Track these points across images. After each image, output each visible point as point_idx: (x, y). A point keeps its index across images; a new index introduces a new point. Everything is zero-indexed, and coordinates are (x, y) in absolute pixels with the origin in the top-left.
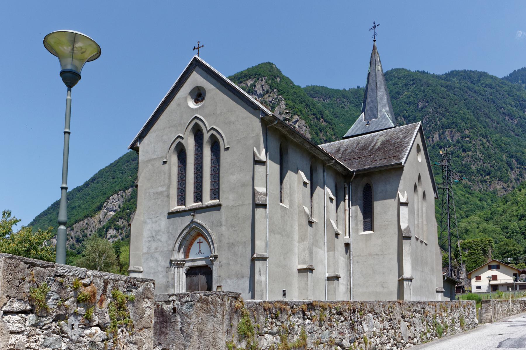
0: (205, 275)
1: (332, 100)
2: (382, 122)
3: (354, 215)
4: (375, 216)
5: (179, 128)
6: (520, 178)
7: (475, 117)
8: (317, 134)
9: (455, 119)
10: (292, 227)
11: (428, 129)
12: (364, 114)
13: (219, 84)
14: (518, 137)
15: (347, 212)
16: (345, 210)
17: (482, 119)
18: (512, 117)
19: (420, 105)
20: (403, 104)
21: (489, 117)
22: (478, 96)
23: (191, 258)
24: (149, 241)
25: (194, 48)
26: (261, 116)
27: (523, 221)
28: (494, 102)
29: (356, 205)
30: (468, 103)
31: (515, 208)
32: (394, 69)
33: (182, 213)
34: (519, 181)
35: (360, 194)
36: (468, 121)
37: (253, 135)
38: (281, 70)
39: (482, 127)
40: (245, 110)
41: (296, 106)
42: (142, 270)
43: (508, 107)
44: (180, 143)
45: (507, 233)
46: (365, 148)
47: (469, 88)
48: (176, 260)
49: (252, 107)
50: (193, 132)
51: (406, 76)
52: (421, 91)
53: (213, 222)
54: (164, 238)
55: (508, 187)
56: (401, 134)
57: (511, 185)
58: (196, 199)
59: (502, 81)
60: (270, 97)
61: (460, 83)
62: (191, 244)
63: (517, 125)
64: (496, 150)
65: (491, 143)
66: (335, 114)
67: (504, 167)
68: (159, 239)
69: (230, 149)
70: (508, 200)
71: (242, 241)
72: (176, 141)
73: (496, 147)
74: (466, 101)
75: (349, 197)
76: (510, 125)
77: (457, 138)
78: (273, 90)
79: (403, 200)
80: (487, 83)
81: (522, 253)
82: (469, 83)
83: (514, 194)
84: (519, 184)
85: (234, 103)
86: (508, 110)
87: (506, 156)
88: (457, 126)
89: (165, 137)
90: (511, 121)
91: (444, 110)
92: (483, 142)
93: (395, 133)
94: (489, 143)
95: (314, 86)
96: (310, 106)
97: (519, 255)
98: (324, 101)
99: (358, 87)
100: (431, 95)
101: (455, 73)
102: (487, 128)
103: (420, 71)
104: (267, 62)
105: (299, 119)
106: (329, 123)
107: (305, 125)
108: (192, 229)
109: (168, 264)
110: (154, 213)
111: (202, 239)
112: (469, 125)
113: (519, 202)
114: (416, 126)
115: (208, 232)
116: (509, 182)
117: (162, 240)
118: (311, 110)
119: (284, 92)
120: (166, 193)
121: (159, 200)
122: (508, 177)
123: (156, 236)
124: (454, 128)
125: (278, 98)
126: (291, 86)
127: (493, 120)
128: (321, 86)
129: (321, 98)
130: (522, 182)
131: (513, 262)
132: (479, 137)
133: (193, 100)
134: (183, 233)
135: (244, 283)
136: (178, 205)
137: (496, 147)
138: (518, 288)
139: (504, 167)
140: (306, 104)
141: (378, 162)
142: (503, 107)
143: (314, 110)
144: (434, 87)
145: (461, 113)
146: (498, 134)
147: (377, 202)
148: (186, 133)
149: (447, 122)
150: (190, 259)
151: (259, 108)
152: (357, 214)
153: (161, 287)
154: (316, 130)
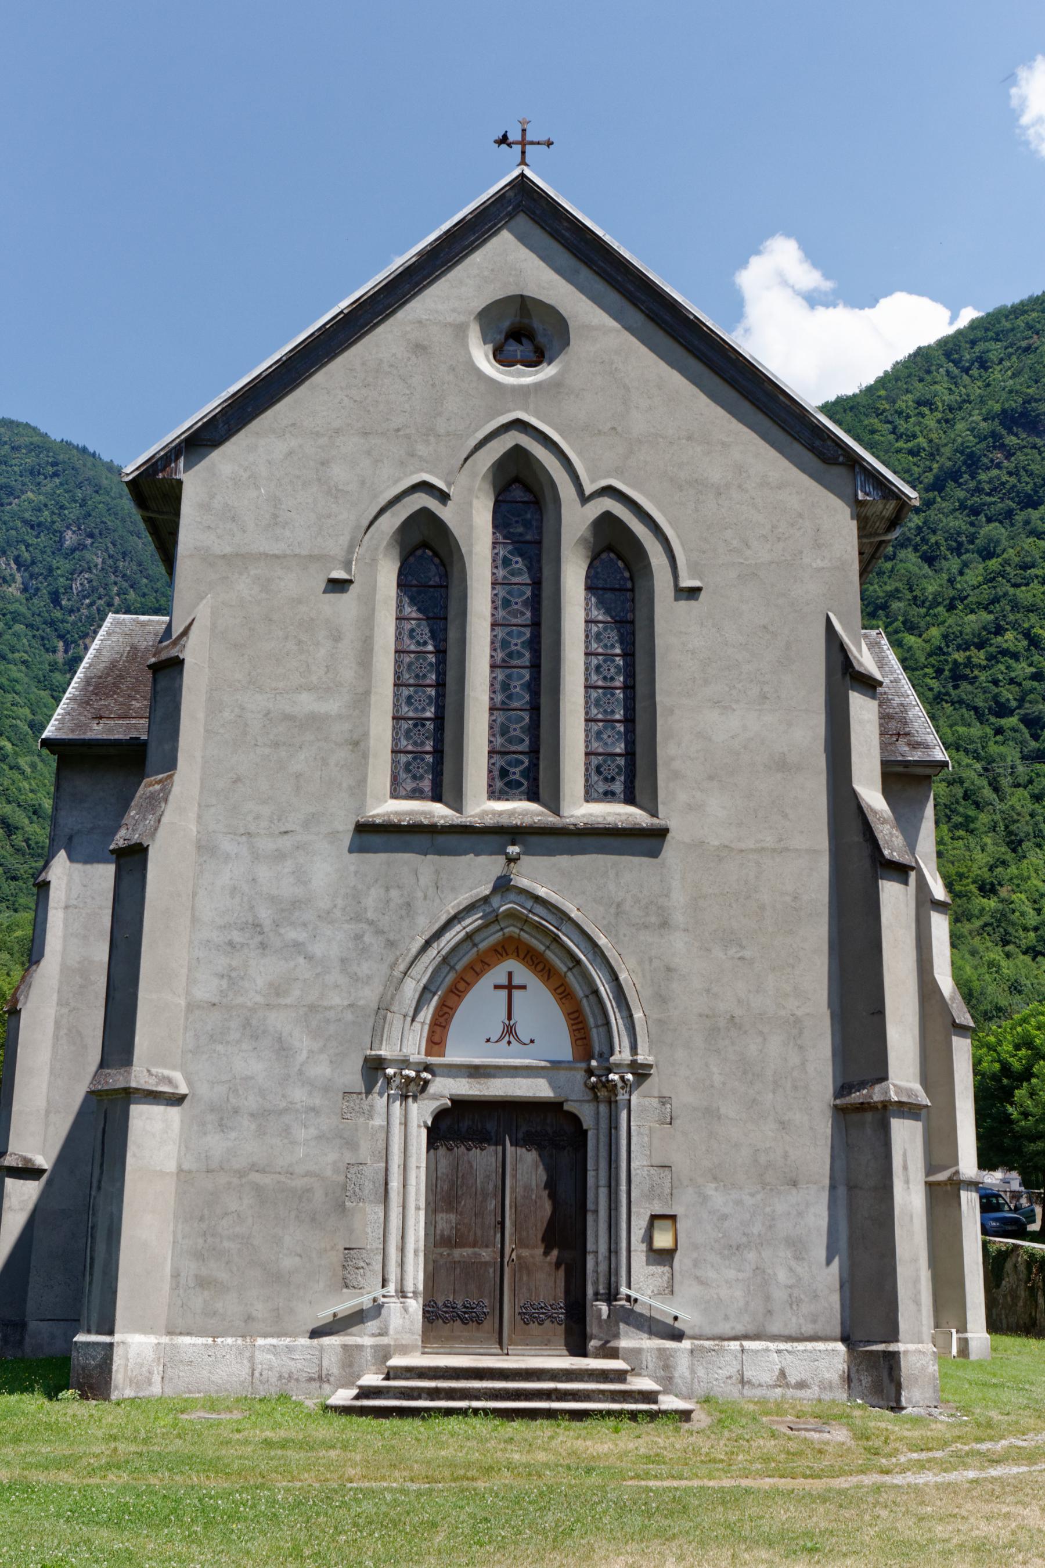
0: (540, 1148)
5: (422, 449)
11: (85, 611)
19: (70, 538)
20: (19, 524)
23: (453, 1056)
24: (231, 944)
25: (504, 140)
33: (441, 839)
37: (819, 563)
40: (773, 453)
42: (183, 1089)
48: (405, 1063)
49: (812, 449)
52: (75, 501)
53: (619, 905)
58: (499, 784)
62: (457, 991)
68: (297, 946)
69: (703, 594)
71: (783, 1013)
72: (407, 500)
89: (339, 473)
91: (135, 568)
100: (104, 519)
103: (75, 444)
109: (353, 1076)
111: (522, 974)
115: (595, 945)
134: (448, 936)
135: (800, 1214)
136: (395, 795)
144: (114, 499)
148: (463, 479)
149: (142, 603)
150: (447, 1059)
151: (854, 462)
153: (309, 1190)
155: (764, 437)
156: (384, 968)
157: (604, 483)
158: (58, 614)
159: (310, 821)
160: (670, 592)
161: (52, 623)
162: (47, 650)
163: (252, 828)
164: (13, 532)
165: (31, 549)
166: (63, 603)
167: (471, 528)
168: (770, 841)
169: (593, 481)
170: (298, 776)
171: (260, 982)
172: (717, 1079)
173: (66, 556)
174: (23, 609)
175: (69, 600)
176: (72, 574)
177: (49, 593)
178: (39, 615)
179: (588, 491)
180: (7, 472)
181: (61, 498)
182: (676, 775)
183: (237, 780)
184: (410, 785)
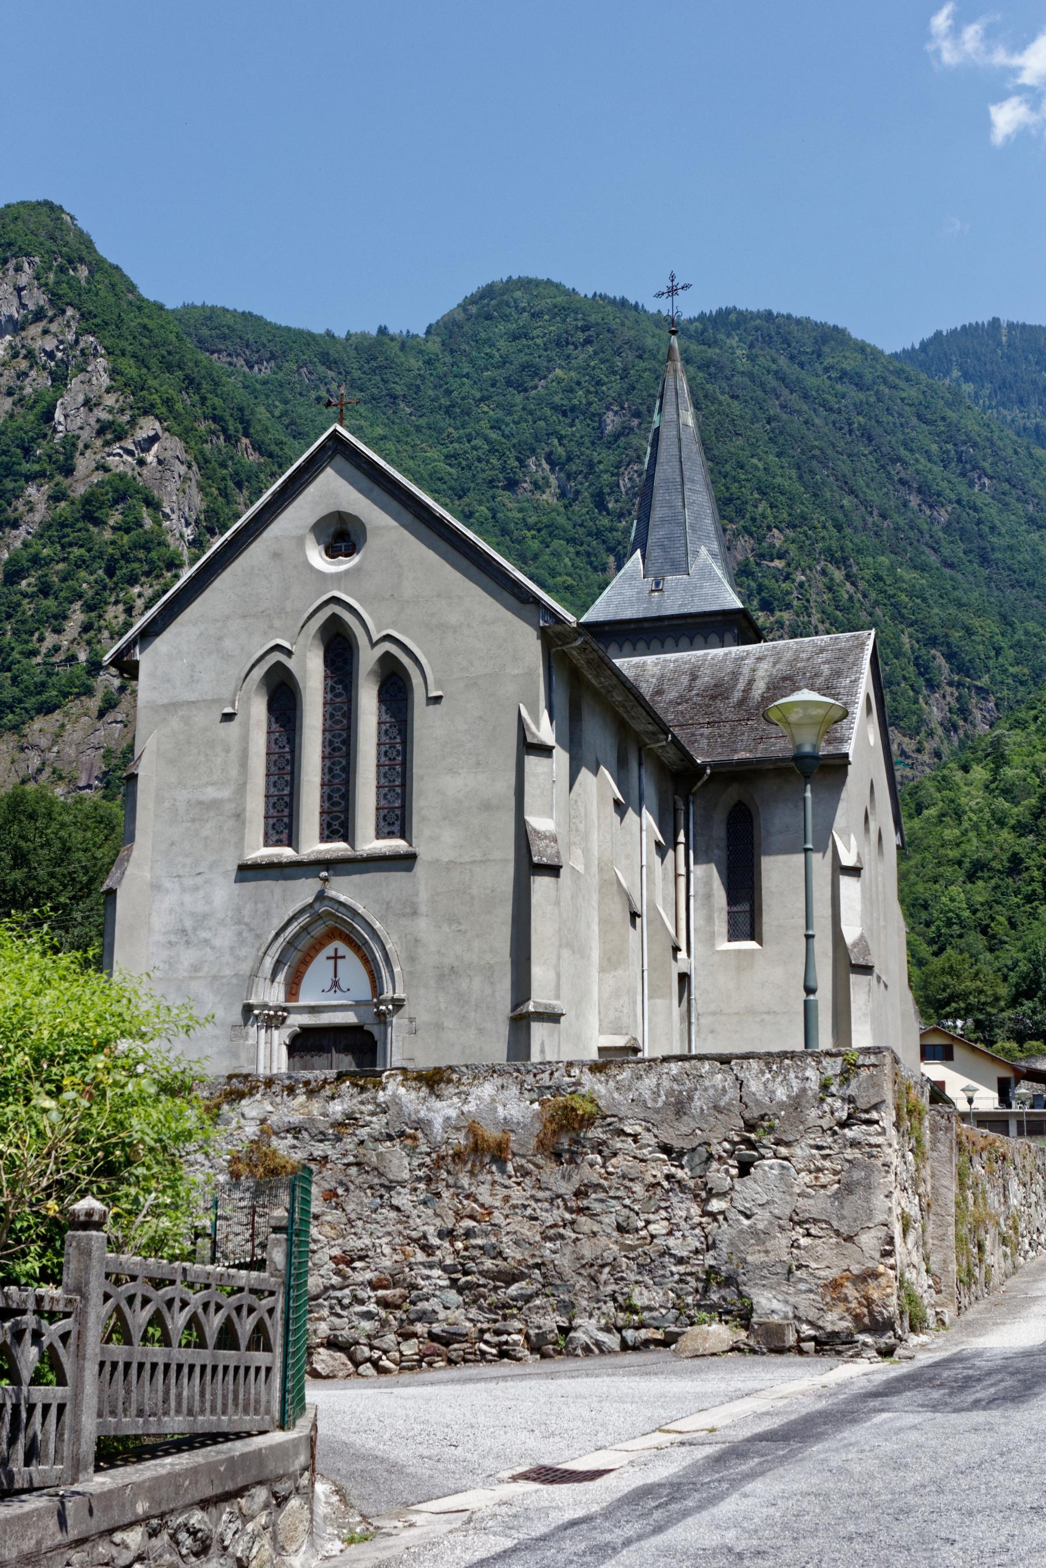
0: (353, 1054)
1: (280, 368)
2: (701, 587)
3: (701, 891)
4: (764, 897)
5: (277, 623)
6: (961, 723)
7: (806, 487)
8: (224, 493)
9: (734, 488)
10: (589, 925)
12: (643, 557)
13: (408, 517)
14: (953, 573)
15: (682, 881)
16: (677, 876)
17: (828, 495)
18: (930, 497)
19: (612, 422)
20: (548, 412)
21: (852, 492)
22: (815, 411)
23: (303, 1001)
24: (170, 943)
26: (542, 623)
27: (980, 883)
28: (870, 439)
29: (708, 862)
30: (781, 433)
31: (951, 833)
32: (515, 277)
33: (286, 871)
34: (956, 731)
35: (719, 831)
36: (782, 498)
37: (516, 672)
38: (94, 238)
39: (829, 524)
40: (490, 600)
41: (151, 382)
43: (917, 460)
44: (279, 665)
45: (928, 925)
46: (719, 691)
47: (783, 379)
48: (265, 1006)
49: (514, 595)
50: (323, 640)
51: (560, 312)
52: (614, 373)
54: (225, 938)
55: (919, 751)
56: (824, 663)
57: (929, 746)
58: (326, 832)
59: (897, 364)
60: (48, 337)
61: (753, 359)
62: (305, 962)
63: (947, 528)
64: (878, 612)
65: (862, 585)
66: (292, 423)
67: (905, 678)
68: (206, 941)
70: (926, 801)
72: (268, 658)
73: (877, 603)
74: (773, 424)
75: (687, 836)
76: (926, 527)
77: (740, 558)
78: (63, 312)
79: (848, 859)
80: (846, 366)
81: (1002, 1003)
82: (783, 361)
83: (944, 783)
84: (956, 744)
85: (458, 575)
86: (918, 472)
87: (911, 637)
88: (740, 512)
89: (228, 643)
90: (928, 512)
92: (832, 579)
93: (804, 656)
94: (853, 584)
95: (213, 308)
96: (199, 384)
97: (994, 1011)
98: (251, 368)
99: (382, 331)
101: (733, 317)
102: (848, 531)
103: (612, 296)
104: (41, 199)
105: (160, 433)
106: (271, 455)
107: (184, 456)
108: (317, 918)
109: (236, 1015)
110: (188, 861)
111: (343, 949)
112: (785, 515)
113: (965, 812)
114: (863, 644)
115: (373, 930)
116: (923, 734)
117: (217, 942)
118: (203, 400)
119: (107, 324)
120: (230, 808)
121: (208, 825)
122: (918, 713)
123: (195, 929)
124: (731, 521)
125: (82, 345)
126: (130, 303)
127: (865, 503)
128: (240, 310)
129: (238, 355)
130: (966, 736)
131: (973, 1036)
132: (818, 561)
133: (322, 548)
134: (290, 929)
136: (266, 844)
137: (877, 603)
138: (1013, 1129)
139: (905, 678)
140: (187, 377)
141: (774, 745)
142: (899, 459)
143: (217, 401)
145: (756, 468)
146: (883, 554)
147: (772, 858)
148: (301, 640)
150: (302, 1002)
151: (537, 601)
152: (711, 889)
154: (224, 479)
155: (485, 589)
156: (254, 951)
157: (384, 633)
158: (605, 521)
159: (212, 866)
160: (424, 701)
161: (598, 534)
162: (595, 569)
163: (181, 873)
164: (542, 423)
165: (565, 442)
166: (610, 506)
167: (305, 671)
168: (478, 855)
169: (378, 632)
170: (206, 838)
171: (186, 964)
172: (443, 1006)
173: (609, 446)
174: (561, 520)
175: (616, 501)
176: (618, 467)
177: (592, 495)
178: (581, 525)
179: (375, 638)
180: (529, 347)
181: (597, 372)
182: (424, 819)
183: (173, 844)
184: (275, 838)
